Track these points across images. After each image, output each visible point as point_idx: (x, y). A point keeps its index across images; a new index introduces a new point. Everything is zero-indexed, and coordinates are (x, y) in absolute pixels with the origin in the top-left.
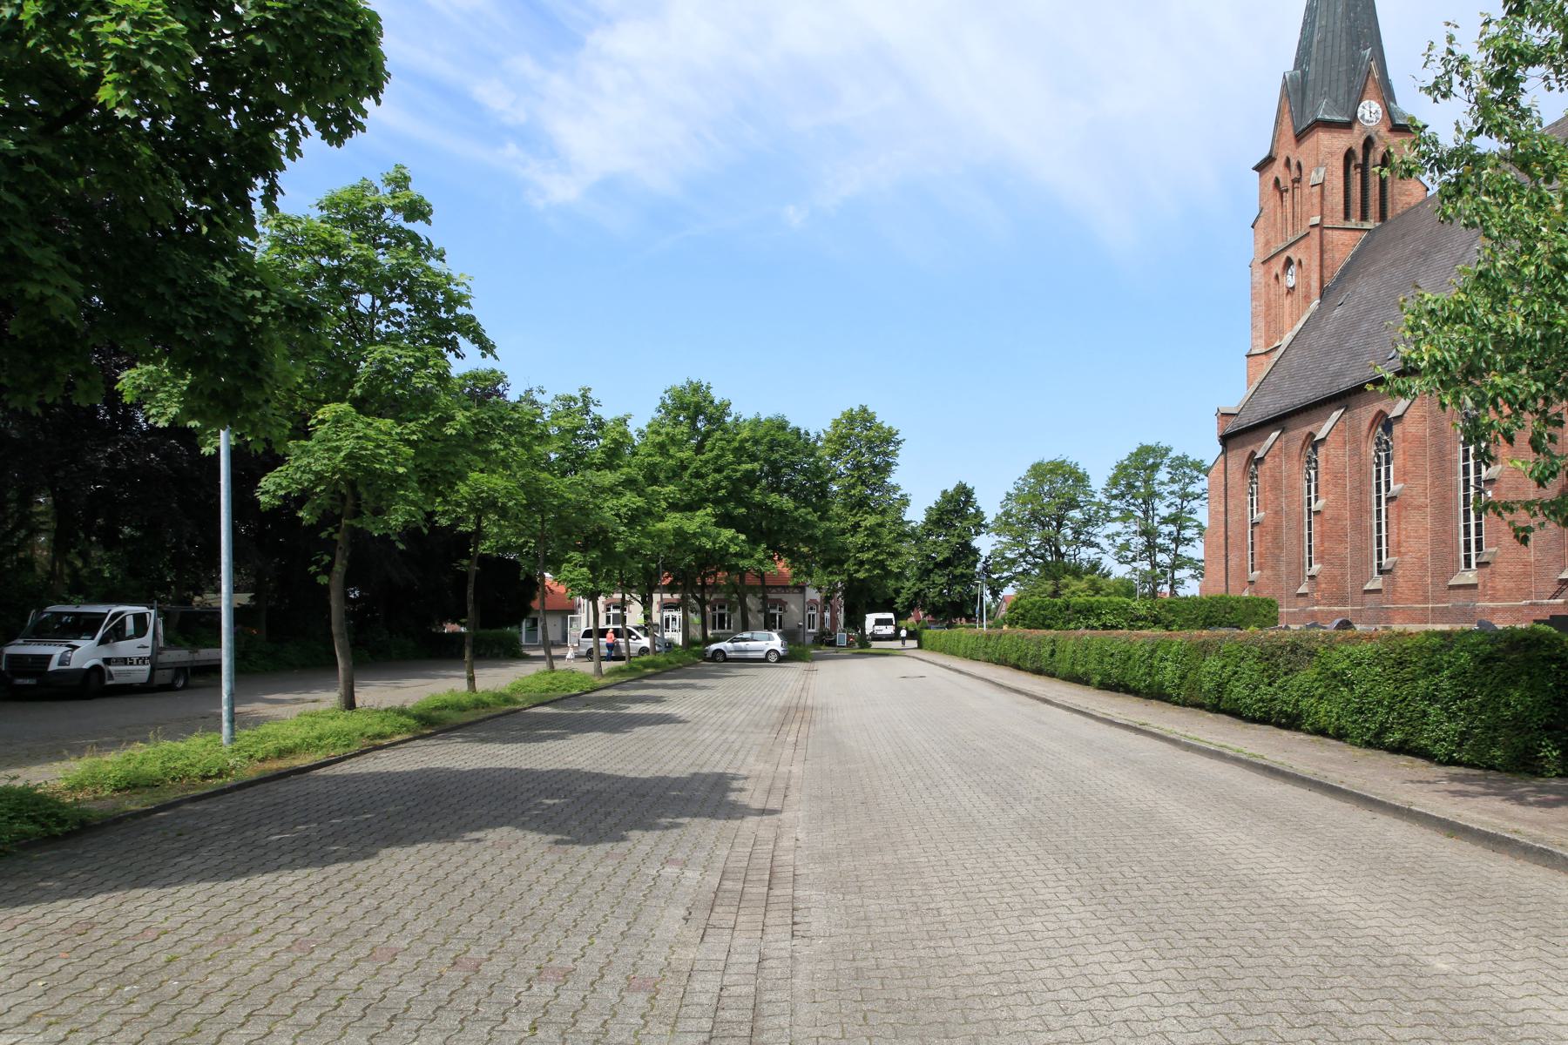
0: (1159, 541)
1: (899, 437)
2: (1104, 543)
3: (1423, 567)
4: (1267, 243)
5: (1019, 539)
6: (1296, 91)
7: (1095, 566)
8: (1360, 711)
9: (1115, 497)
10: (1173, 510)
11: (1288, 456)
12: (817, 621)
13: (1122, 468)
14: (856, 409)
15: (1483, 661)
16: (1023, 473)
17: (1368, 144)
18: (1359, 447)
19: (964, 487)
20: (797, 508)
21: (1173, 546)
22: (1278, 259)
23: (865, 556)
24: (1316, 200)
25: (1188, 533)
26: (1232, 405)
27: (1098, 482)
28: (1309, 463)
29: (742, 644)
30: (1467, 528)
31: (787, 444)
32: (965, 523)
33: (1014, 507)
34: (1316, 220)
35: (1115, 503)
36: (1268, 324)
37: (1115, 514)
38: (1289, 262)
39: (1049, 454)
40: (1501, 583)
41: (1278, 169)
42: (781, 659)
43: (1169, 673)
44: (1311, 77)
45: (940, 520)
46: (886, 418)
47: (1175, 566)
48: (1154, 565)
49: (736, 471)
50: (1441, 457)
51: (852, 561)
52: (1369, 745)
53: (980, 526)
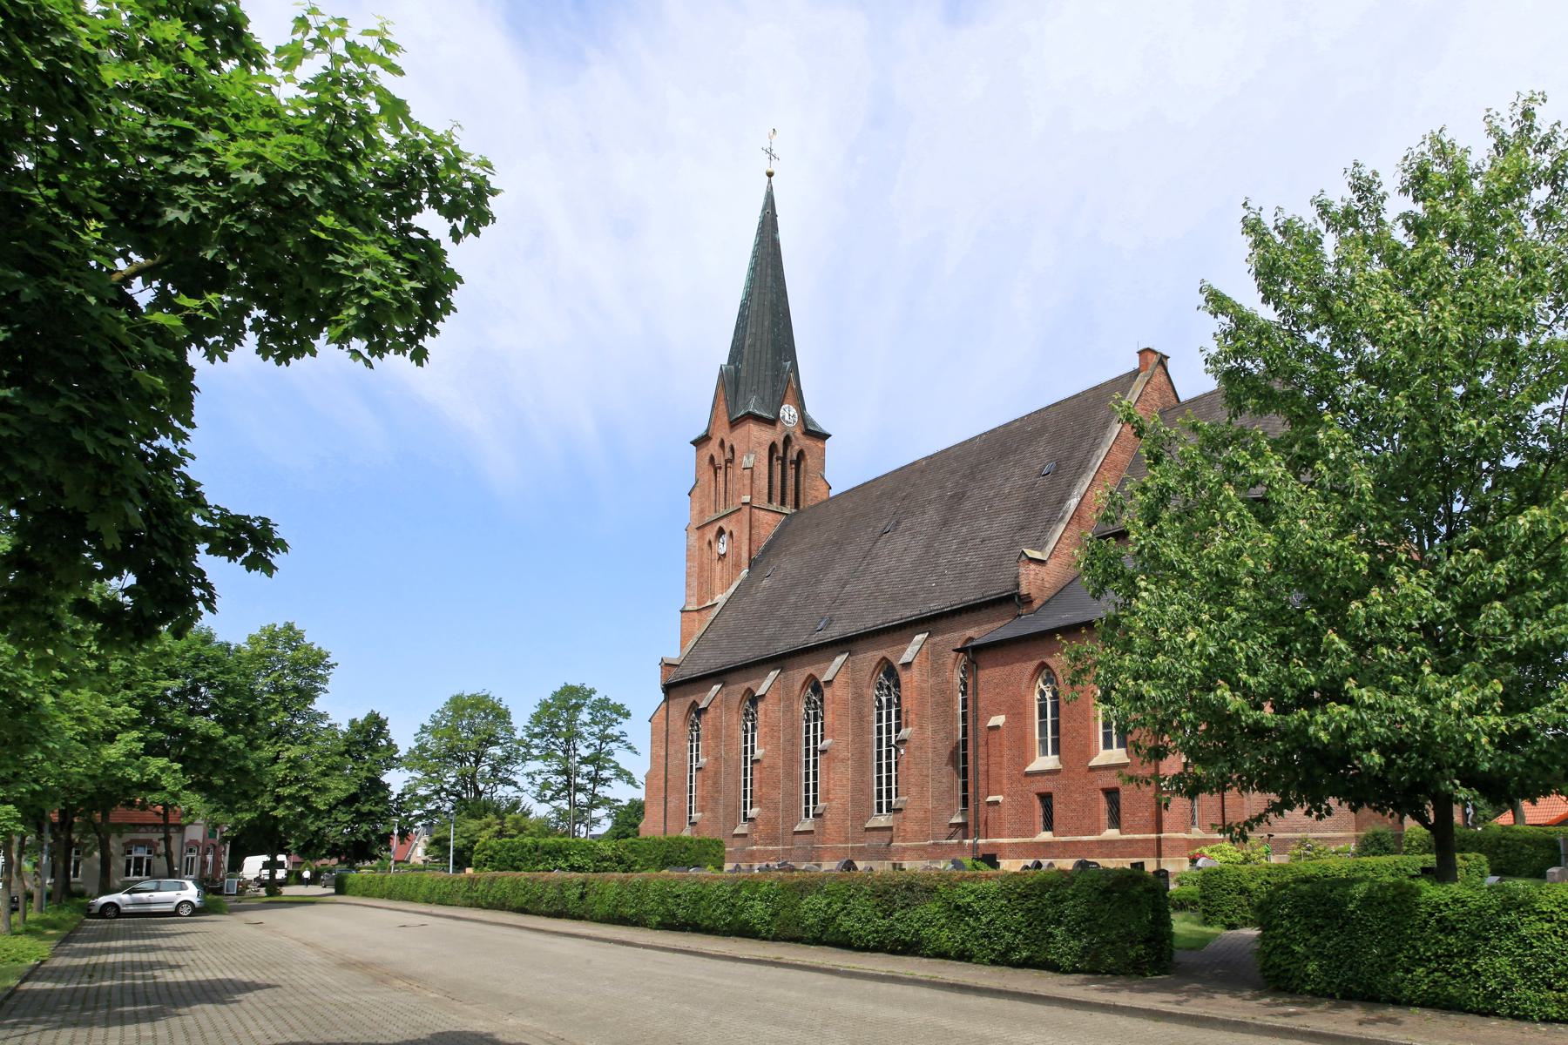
0: (579, 780)
1: (331, 660)
2: (523, 782)
3: (845, 812)
4: (702, 511)
5: (432, 775)
6: (731, 383)
7: (515, 805)
8: (986, 936)
9: (536, 735)
10: (592, 750)
11: (728, 708)
12: (197, 865)
13: (545, 706)
14: (280, 625)
15: (1102, 893)
16: (441, 706)
17: (787, 441)
18: (792, 704)
19: (377, 717)
20: (225, 736)
21: (590, 786)
22: (709, 527)
23: (286, 791)
24: (747, 482)
25: (605, 774)
26: (674, 655)
27: (520, 720)
28: (746, 715)
29: (144, 896)
30: (880, 779)
31: (217, 661)
32: (376, 756)
33: (430, 741)
34: (747, 499)
35: (536, 741)
36: (700, 585)
37: (535, 752)
38: (721, 532)
39: (470, 687)
40: (911, 827)
41: (713, 447)
42: (196, 911)
43: (758, 911)
44: (743, 374)
45: (347, 751)
46: (315, 637)
47: (592, 806)
48: (573, 804)
49: (154, 689)
50: (861, 718)
51: (267, 796)
52: (993, 963)
53: (391, 759)
